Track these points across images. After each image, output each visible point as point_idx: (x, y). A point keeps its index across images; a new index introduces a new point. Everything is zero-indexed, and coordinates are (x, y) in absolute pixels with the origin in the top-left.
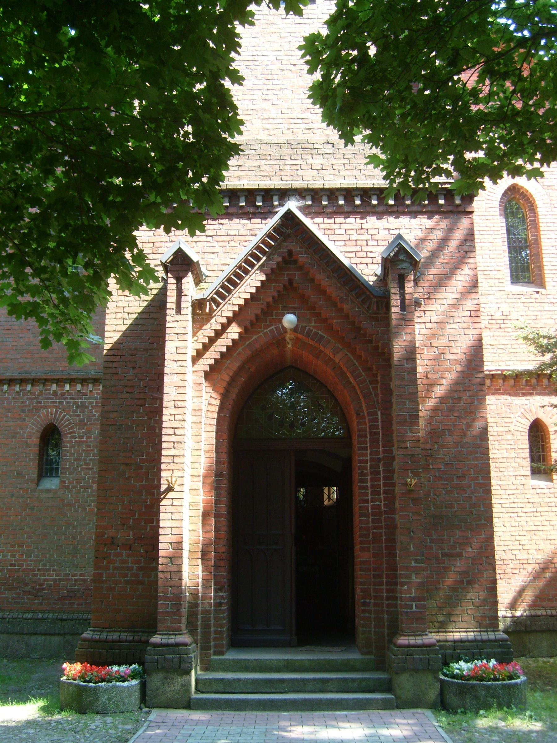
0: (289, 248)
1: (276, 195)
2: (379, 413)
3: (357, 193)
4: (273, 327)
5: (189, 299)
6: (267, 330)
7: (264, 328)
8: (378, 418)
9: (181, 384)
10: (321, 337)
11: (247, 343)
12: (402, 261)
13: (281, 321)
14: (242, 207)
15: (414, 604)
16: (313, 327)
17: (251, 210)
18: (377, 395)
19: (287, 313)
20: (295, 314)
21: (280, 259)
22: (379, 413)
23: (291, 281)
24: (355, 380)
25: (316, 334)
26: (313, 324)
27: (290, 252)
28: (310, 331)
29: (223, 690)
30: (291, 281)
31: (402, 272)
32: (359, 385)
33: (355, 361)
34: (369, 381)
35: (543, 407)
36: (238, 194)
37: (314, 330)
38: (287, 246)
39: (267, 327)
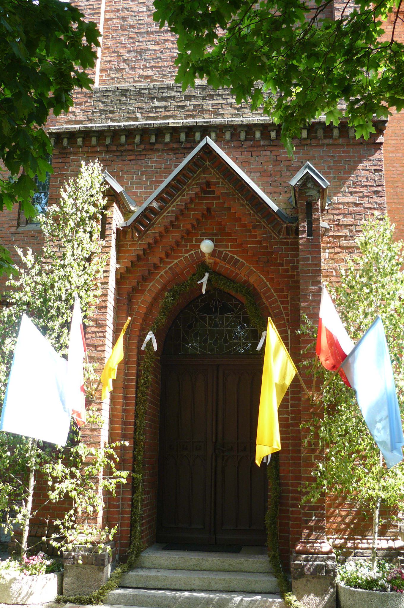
0: (207, 179)
1: (198, 131)
2: (289, 331)
3: (273, 128)
4: (193, 252)
5: (114, 227)
6: (187, 255)
7: (185, 253)
8: (287, 336)
9: (103, 304)
10: (237, 261)
11: (169, 267)
12: (309, 188)
13: (199, 247)
14: (167, 143)
15: (313, 512)
16: (229, 251)
17: (175, 146)
18: (287, 315)
19: (206, 239)
20: (212, 240)
21: (199, 190)
22: (289, 331)
23: (209, 210)
24: (267, 300)
25: (232, 258)
26: (229, 249)
27: (208, 184)
28: (226, 255)
29: (135, 586)
30: (209, 210)
31: (310, 199)
32: (270, 305)
33: (268, 283)
34: (281, 301)
35: (31, 586)
36: (164, 132)
37: (230, 254)
38: (205, 178)
39: (187, 252)
